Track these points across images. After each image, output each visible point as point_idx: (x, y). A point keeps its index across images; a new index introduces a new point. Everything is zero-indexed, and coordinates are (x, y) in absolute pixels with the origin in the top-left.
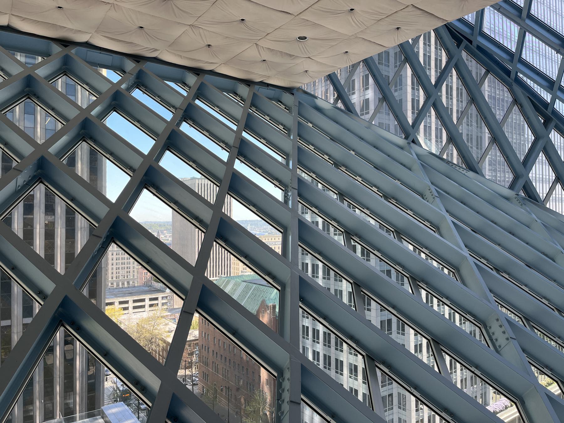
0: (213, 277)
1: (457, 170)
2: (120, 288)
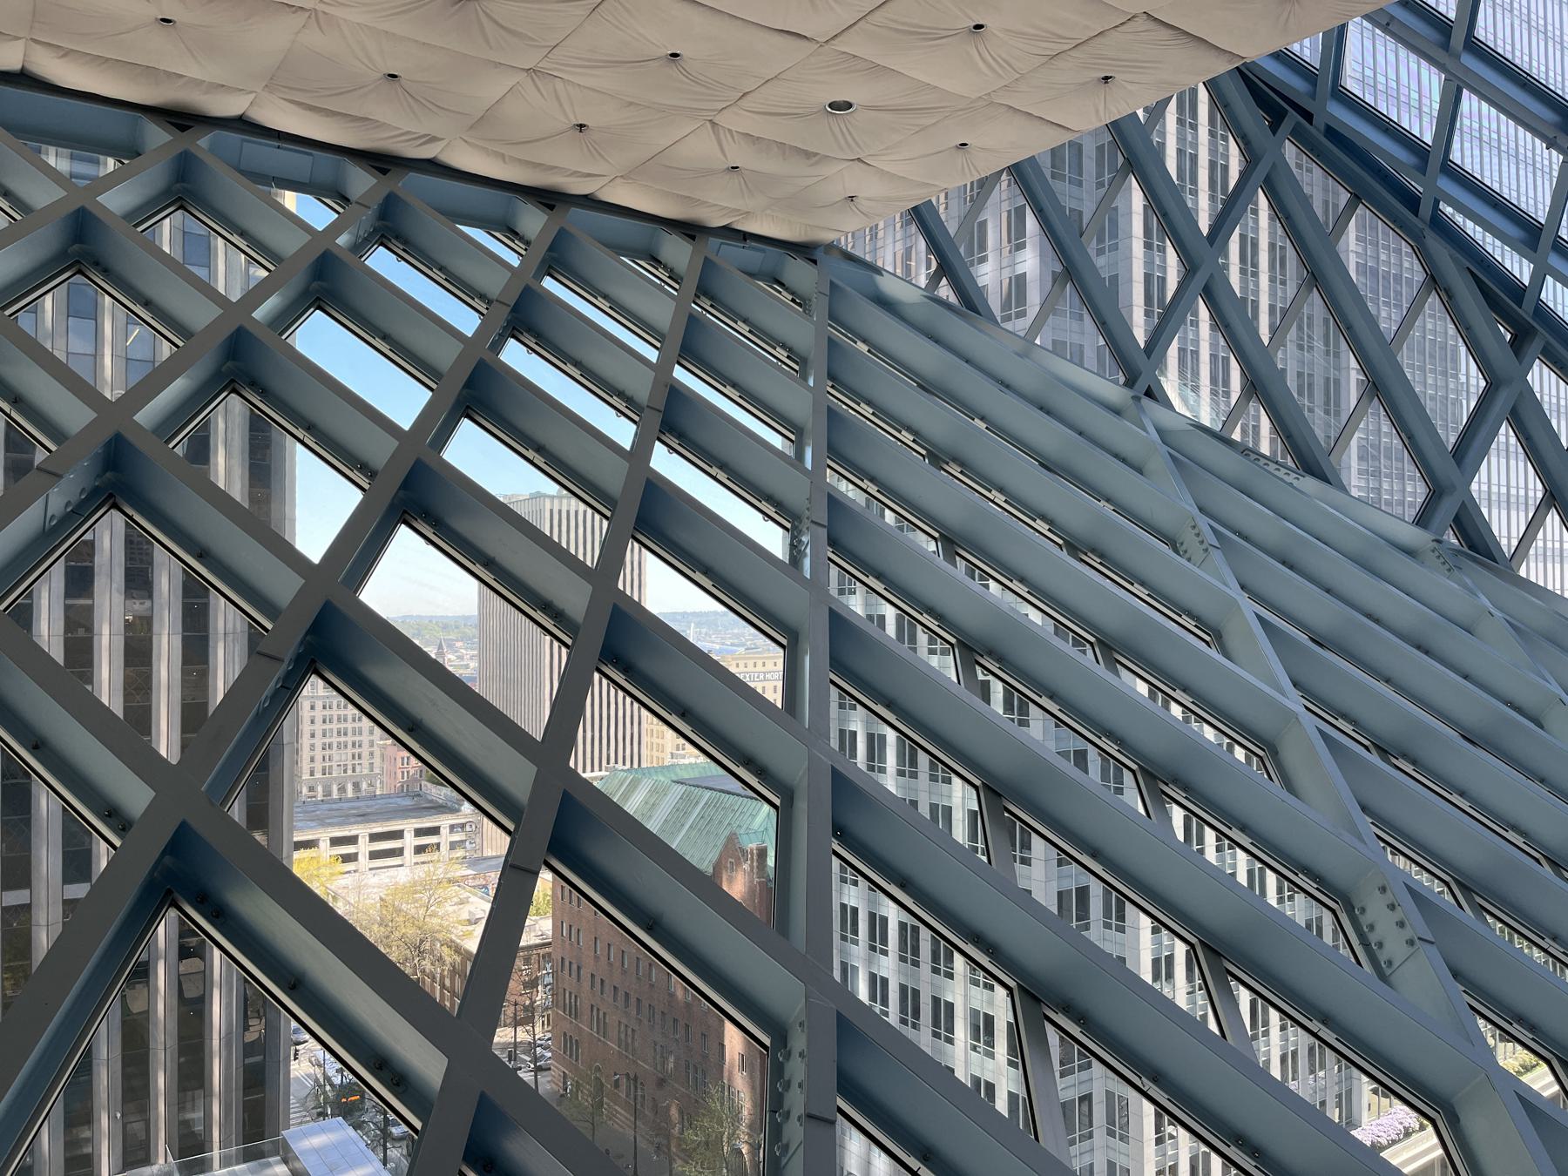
0: (592, 771)
1: (1270, 472)
2: (335, 801)
